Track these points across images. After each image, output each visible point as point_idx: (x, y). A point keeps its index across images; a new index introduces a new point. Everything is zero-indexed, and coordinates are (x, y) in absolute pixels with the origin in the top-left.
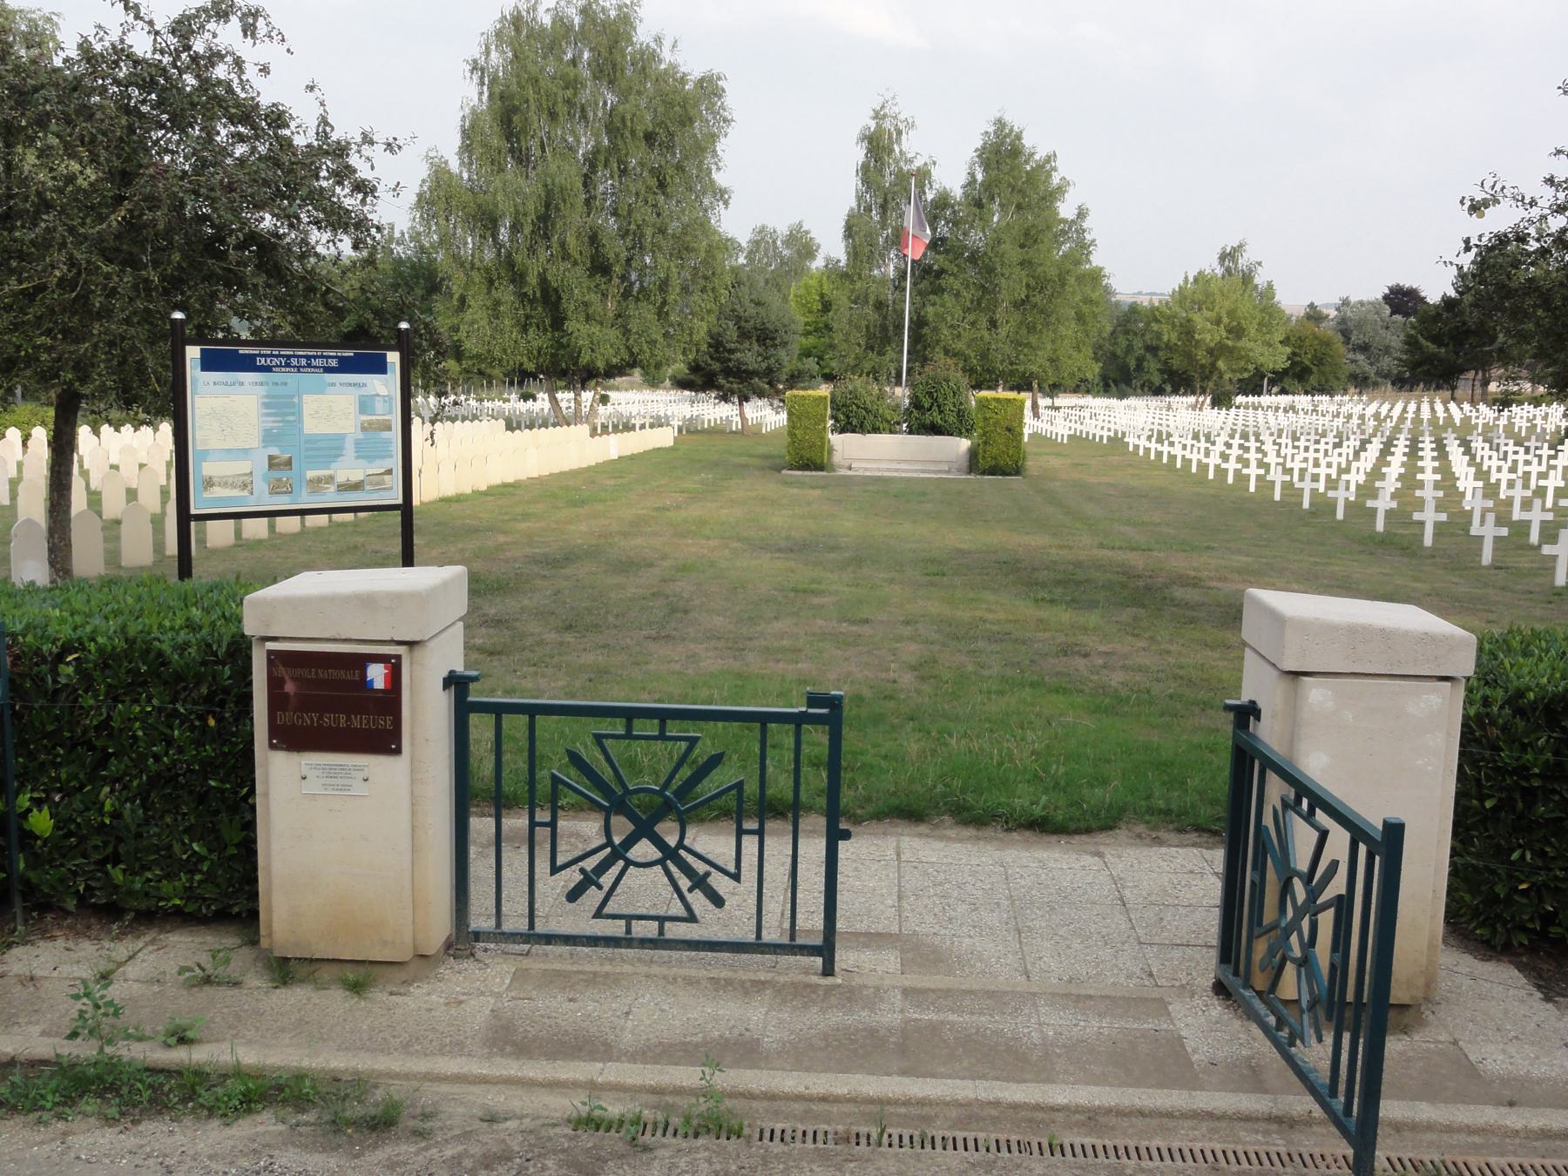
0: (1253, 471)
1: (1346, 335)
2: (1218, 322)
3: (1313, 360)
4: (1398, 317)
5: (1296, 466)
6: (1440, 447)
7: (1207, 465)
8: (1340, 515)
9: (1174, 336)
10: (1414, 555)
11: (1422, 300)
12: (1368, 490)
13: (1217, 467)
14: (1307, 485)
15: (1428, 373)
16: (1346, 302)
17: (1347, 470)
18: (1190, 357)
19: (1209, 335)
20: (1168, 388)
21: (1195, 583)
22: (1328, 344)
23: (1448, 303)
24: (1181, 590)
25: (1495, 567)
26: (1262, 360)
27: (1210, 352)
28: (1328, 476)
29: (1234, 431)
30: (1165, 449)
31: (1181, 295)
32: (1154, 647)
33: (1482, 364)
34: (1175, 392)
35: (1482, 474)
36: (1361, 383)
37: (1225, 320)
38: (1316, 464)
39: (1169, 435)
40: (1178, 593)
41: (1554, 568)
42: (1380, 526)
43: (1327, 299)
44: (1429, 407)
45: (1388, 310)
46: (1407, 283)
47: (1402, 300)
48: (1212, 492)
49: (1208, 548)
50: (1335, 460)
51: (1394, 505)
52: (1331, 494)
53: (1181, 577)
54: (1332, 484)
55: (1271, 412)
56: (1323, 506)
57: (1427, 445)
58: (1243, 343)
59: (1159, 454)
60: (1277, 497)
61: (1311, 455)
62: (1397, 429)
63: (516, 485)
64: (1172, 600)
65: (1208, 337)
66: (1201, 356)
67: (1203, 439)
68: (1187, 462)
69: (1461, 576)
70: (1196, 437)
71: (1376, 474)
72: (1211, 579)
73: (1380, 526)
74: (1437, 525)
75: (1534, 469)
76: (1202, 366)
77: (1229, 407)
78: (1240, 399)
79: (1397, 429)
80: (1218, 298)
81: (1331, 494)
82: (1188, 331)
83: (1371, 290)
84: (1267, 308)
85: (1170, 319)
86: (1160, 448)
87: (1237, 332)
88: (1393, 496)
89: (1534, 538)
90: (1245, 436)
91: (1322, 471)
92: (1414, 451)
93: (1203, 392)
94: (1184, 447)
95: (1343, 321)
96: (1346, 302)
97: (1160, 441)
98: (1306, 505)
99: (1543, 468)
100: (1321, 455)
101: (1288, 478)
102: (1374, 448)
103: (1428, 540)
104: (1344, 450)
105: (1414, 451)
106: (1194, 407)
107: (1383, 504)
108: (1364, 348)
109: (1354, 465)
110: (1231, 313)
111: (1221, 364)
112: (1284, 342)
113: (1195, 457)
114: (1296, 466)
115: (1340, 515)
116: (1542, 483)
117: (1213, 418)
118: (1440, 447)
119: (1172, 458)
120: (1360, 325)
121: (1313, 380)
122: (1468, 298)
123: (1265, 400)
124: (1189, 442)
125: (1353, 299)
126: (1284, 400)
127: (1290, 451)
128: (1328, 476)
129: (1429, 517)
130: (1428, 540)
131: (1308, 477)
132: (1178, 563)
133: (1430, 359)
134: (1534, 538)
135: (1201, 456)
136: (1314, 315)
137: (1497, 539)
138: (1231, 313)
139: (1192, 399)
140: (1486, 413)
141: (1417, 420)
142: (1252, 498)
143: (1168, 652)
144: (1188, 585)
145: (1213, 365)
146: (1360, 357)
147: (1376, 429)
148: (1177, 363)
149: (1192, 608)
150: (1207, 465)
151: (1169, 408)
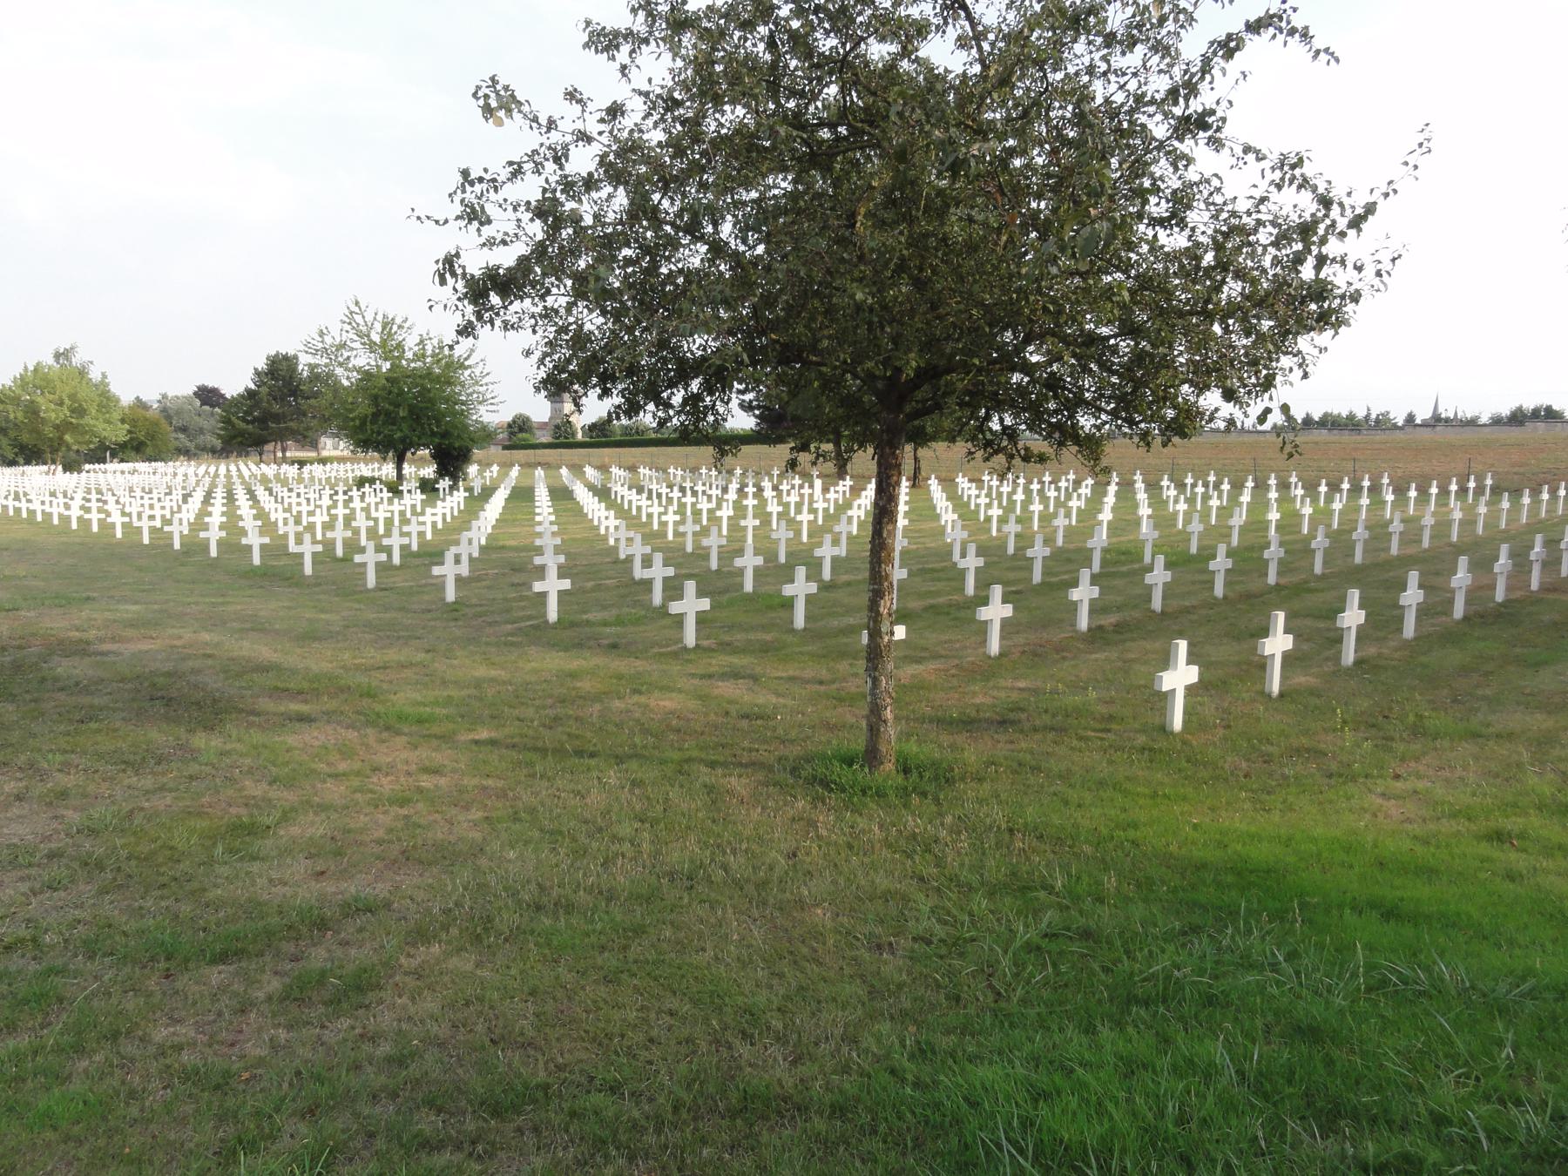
0: (94, 517)
1: (168, 418)
2: (61, 404)
3: (147, 436)
4: (207, 408)
5: (134, 510)
6: (252, 496)
7: (69, 517)
8: (214, 553)
9: (20, 415)
10: (297, 585)
11: (222, 396)
12: (199, 524)
13: (80, 519)
14: (145, 524)
15: (241, 443)
16: (164, 396)
17: (179, 510)
18: (36, 431)
19: (51, 413)
20: (21, 461)
21: (80, 649)
22: (157, 424)
23: (250, 394)
24: (65, 662)
25: (380, 588)
26: (105, 434)
27: (57, 427)
28: (163, 516)
29: (89, 491)
30: (23, 505)
31: (23, 381)
32: (39, 789)
33: (281, 437)
34: (28, 463)
35: (261, 515)
36: (187, 453)
37: (67, 401)
38: (151, 507)
39: (25, 494)
40: (64, 667)
41: (365, 573)
42: (257, 560)
43: (151, 396)
44: (246, 468)
45: (198, 403)
46: (210, 384)
47: (207, 395)
48: (78, 540)
49: (88, 598)
50: (167, 504)
51: (223, 534)
52: (166, 529)
53: (61, 642)
54: (167, 522)
55: (113, 475)
56: (193, 547)
57: (219, 494)
58: (87, 420)
59: (18, 510)
60: (146, 541)
61: (146, 502)
62: (213, 485)
63: (1382, 423)
64: (56, 679)
65: (53, 415)
66: (49, 431)
67: (60, 496)
68: (47, 516)
69: (359, 602)
70: (53, 494)
71: (204, 513)
72: (101, 640)
73: (257, 560)
74: (263, 547)
75: (305, 508)
76: (51, 440)
77: (80, 472)
78: (87, 467)
79: (213, 485)
80: (58, 384)
81: (166, 529)
82: (32, 410)
83: (183, 387)
84: (106, 399)
85: (16, 400)
86: (17, 504)
87: (80, 411)
88: (221, 528)
89: (657, 598)
90: (99, 492)
91: (158, 512)
92: (230, 497)
93: (54, 462)
94: (43, 503)
95: (164, 410)
96: (164, 396)
97: (17, 498)
98: (177, 546)
99: (311, 508)
100: (155, 501)
101: (127, 519)
102: (199, 496)
103: (308, 570)
104: (174, 497)
105: (230, 497)
106: (47, 473)
107: (214, 535)
108: (184, 430)
109: (184, 507)
110: (72, 397)
111: (67, 437)
112: (123, 421)
113: (55, 511)
114: (134, 510)
115: (214, 553)
116: (311, 519)
117: (62, 479)
118: (252, 496)
119: (32, 513)
120: (179, 412)
121: (149, 451)
122: (264, 390)
123: (110, 466)
124: (47, 499)
125: (170, 395)
126: (124, 466)
127: (127, 500)
128: (163, 516)
129: (254, 540)
130: (308, 570)
131: (145, 517)
132: (57, 624)
133: (242, 433)
134: (657, 598)
135: (62, 510)
136: (140, 404)
137: (314, 554)
138: (72, 397)
139: (45, 468)
140: (291, 471)
141: (228, 476)
142: (120, 543)
143: (63, 795)
144: (75, 653)
145: (61, 438)
146: (181, 436)
147: (197, 484)
148: (25, 438)
149: (86, 691)
150: (69, 517)
151: (23, 473)
